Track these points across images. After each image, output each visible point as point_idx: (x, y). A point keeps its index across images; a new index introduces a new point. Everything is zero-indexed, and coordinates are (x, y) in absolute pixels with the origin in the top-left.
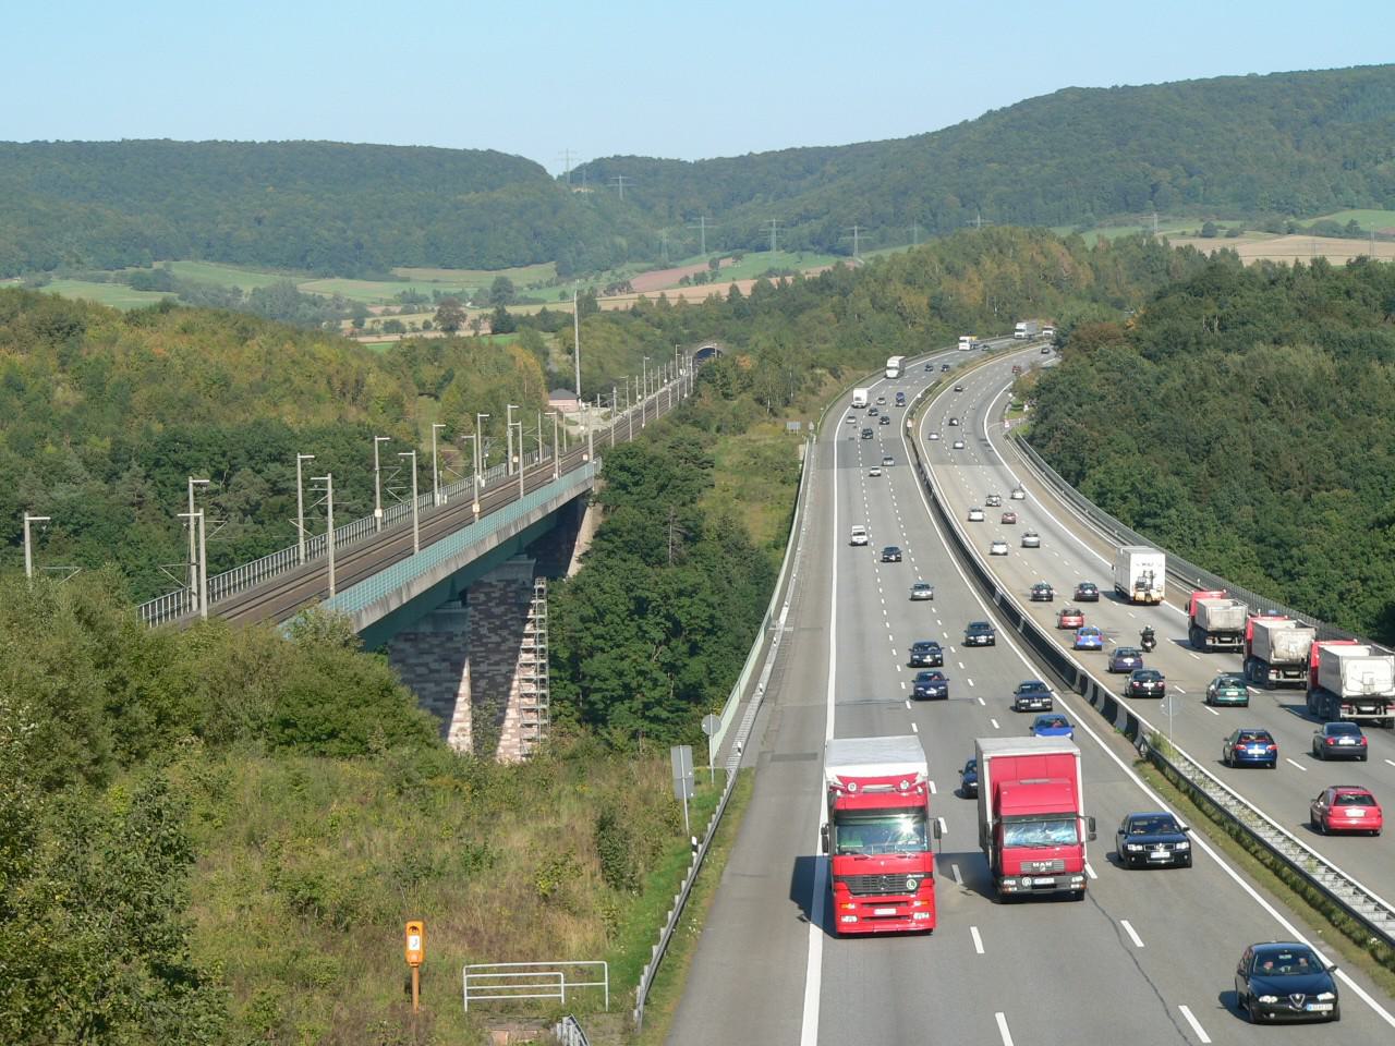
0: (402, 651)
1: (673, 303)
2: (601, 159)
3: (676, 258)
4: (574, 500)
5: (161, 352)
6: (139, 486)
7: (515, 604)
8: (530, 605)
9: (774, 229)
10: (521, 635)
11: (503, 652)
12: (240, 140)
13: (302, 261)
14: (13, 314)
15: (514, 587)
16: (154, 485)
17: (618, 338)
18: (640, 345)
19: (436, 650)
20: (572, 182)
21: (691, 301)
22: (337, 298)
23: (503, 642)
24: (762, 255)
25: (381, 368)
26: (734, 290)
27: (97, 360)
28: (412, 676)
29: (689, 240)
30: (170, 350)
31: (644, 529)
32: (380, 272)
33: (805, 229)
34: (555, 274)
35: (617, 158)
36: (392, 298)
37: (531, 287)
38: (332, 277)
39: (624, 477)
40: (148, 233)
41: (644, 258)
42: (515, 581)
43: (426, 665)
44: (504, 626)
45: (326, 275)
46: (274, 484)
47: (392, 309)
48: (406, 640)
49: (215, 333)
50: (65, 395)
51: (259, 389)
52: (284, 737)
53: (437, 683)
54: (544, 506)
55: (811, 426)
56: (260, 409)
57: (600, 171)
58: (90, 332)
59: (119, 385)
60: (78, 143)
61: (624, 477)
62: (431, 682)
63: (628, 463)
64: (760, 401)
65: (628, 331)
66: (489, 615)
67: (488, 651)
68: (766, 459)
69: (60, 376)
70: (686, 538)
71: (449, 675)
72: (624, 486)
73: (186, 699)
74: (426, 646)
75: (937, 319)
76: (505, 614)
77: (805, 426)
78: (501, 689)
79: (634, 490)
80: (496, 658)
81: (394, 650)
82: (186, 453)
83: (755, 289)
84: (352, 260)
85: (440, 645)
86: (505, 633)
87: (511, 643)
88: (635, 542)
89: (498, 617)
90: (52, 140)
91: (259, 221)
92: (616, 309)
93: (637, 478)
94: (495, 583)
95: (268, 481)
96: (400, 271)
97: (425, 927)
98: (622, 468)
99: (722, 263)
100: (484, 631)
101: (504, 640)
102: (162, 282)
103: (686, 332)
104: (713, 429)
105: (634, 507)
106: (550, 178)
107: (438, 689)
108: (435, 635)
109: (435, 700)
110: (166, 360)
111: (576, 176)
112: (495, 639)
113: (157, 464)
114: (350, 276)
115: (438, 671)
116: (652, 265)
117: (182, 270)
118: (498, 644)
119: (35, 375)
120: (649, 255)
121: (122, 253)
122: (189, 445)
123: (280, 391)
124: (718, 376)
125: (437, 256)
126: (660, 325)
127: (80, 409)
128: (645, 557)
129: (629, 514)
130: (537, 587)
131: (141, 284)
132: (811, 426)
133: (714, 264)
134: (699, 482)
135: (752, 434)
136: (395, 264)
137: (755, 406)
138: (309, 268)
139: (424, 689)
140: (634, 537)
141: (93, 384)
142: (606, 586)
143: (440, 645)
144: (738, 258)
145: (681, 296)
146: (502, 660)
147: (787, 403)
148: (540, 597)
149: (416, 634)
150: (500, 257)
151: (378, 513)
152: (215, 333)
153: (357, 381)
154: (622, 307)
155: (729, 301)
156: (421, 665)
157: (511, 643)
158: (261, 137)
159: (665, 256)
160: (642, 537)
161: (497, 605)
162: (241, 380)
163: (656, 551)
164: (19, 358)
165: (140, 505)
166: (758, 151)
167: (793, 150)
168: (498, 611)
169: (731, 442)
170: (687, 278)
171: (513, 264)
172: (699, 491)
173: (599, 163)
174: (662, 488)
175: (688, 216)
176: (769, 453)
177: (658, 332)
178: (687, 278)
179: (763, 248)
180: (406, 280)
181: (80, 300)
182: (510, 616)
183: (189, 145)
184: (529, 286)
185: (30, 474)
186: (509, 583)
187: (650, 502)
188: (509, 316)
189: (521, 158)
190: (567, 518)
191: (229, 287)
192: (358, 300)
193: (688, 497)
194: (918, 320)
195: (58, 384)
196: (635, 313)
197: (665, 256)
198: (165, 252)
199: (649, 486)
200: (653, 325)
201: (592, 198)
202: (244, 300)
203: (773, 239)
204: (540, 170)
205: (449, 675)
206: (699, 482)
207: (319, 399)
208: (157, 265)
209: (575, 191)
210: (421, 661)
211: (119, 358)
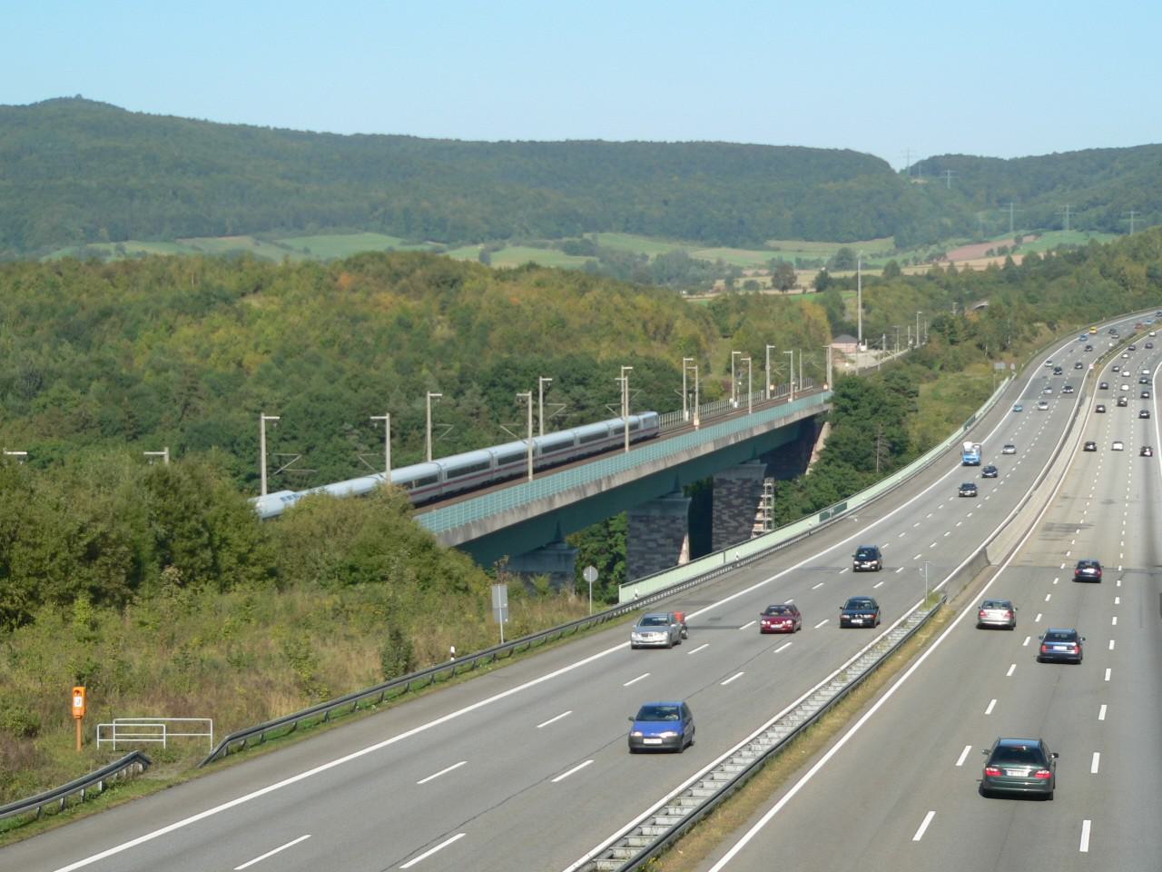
0: (639, 529)
1: (960, 270)
2: (935, 157)
3: (990, 233)
4: (811, 418)
5: (515, 300)
6: (476, 400)
7: (750, 498)
8: (761, 499)
9: (1068, 213)
10: (752, 522)
11: (738, 534)
13: (698, 234)
14: (413, 271)
15: (749, 484)
16: (491, 400)
17: (911, 297)
18: (929, 302)
19: (663, 529)
20: (912, 174)
21: (977, 269)
22: (720, 262)
24: (1057, 234)
25: (687, 316)
26: (1009, 262)
27: (467, 306)
29: (1001, 221)
30: (523, 300)
31: (857, 443)
32: (756, 242)
33: (1092, 213)
34: (893, 247)
35: (948, 156)
36: (764, 263)
37: (873, 256)
38: (720, 246)
39: (845, 402)
40: (581, 211)
41: (965, 234)
42: (749, 480)
43: (655, 540)
44: (741, 514)
45: (715, 245)
46: (578, 401)
47: (760, 272)
48: (641, 521)
49: (561, 287)
50: (442, 331)
51: (587, 330)
52: (351, 579)
53: (664, 555)
54: (771, 423)
55: (1013, 367)
56: (586, 344)
57: (933, 166)
58: (467, 285)
59: (481, 325)
60: (533, 143)
61: (845, 402)
63: (849, 391)
64: (980, 346)
65: (920, 291)
66: (729, 505)
67: (729, 533)
68: (974, 391)
69: (440, 317)
70: (892, 450)
71: (671, 549)
72: (845, 410)
73: (261, 548)
74: (656, 526)
75: (1153, 285)
76: (742, 505)
77: (1008, 367)
79: (853, 412)
82: (514, 377)
83: (1025, 260)
87: (746, 528)
88: (849, 453)
89: (737, 507)
90: (513, 140)
91: (666, 203)
92: (916, 274)
93: (855, 403)
94: (734, 481)
95: (573, 399)
96: (773, 243)
97: (86, 692)
98: (844, 396)
99: (1026, 239)
100: (725, 517)
102: (588, 249)
103: (967, 292)
104: (937, 368)
105: (852, 426)
106: (893, 171)
108: (663, 518)
110: (519, 306)
111: (914, 171)
112: (734, 524)
113: (493, 384)
114: (734, 246)
116: (968, 240)
117: (606, 240)
118: (736, 528)
119: (421, 317)
120: (968, 232)
121: (561, 226)
122: (515, 369)
123: (601, 332)
124: (947, 326)
125: (801, 231)
126: (947, 287)
127: (450, 342)
128: (856, 466)
129: (849, 431)
130: (766, 485)
131: (571, 250)
132: (1013, 367)
134: (904, 408)
135: (967, 373)
136: (768, 237)
137: (976, 350)
138: (702, 239)
140: (848, 449)
141: (463, 324)
142: (822, 486)
144: (1038, 235)
145: (967, 265)
147: (1004, 348)
148: (769, 493)
149: (648, 517)
150: (850, 232)
152: (561, 287)
153: (667, 326)
154: (920, 272)
155: (1005, 269)
157: (746, 528)
158: (671, 138)
159: (980, 233)
160: (855, 449)
161: (737, 498)
162: (575, 322)
163: (865, 460)
164: (412, 304)
165: (477, 415)
166: (1061, 151)
167: (1089, 150)
168: (736, 502)
169: (950, 377)
170: (992, 251)
171: (861, 238)
172: (904, 415)
173: (934, 160)
174: (875, 411)
175: (1002, 201)
176: (977, 387)
177: (945, 292)
178: (992, 251)
179: (1058, 228)
180: (777, 249)
182: (746, 506)
183: (617, 144)
184: (872, 255)
185: (397, 390)
186: (745, 481)
187: (865, 423)
188: (830, 279)
189: (871, 156)
190: (808, 428)
191: (639, 253)
192: (736, 264)
193: (894, 419)
194: (1137, 286)
195: (439, 322)
196: (929, 277)
197: (980, 233)
198: (593, 225)
199: (865, 409)
200: (942, 287)
201: (926, 187)
202: (649, 263)
203: (1066, 221)
204: (885, 165)
205: (671, 549)
206: (904, 408)
207: (632, 338)
208: (587, 236)
209: (913, 181)
211: (485, 304)
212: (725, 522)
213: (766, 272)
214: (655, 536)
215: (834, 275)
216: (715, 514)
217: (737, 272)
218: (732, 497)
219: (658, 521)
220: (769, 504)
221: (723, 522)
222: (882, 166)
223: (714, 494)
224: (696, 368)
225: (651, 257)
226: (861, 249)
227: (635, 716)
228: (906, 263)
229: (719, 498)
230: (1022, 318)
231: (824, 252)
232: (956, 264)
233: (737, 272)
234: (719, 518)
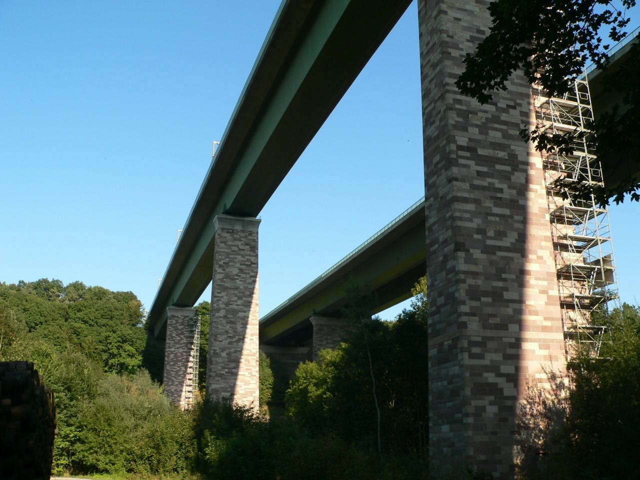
0: (226, 237)
7: (188, 326)
11: (182, 344)
15: (187, 319)
23: (181, 340)
42: (188, 316)
43: (237, 246)
48: (227, 232)
53: (243, 256)
66: (176, 329)
74: (238, 237)
78: (179, 359)
80: (179, 346)
81: (221, 237)
85: (246, 237)
86: (182, 336)
89: (180, 330)
94: (179, 316)
100: (174, 335)
101: (182, 339)
107: (243, 259)
108: (243, 232)
109: (241, 265)
115: (244, 250)
118: (179, 341)
139: (236, 258)
143: (246, 237)
146: (180, 347)
149: (233, 230)
161: (180, 325)
181: (42, 279)
210: (235, 244)
212: (174, 337)
216: (168, 333)
219: (239, 233)
221: (173, 337)
227: (611, 255)
229: (171, 325)
230: (70, 434)
234: (171, 335)
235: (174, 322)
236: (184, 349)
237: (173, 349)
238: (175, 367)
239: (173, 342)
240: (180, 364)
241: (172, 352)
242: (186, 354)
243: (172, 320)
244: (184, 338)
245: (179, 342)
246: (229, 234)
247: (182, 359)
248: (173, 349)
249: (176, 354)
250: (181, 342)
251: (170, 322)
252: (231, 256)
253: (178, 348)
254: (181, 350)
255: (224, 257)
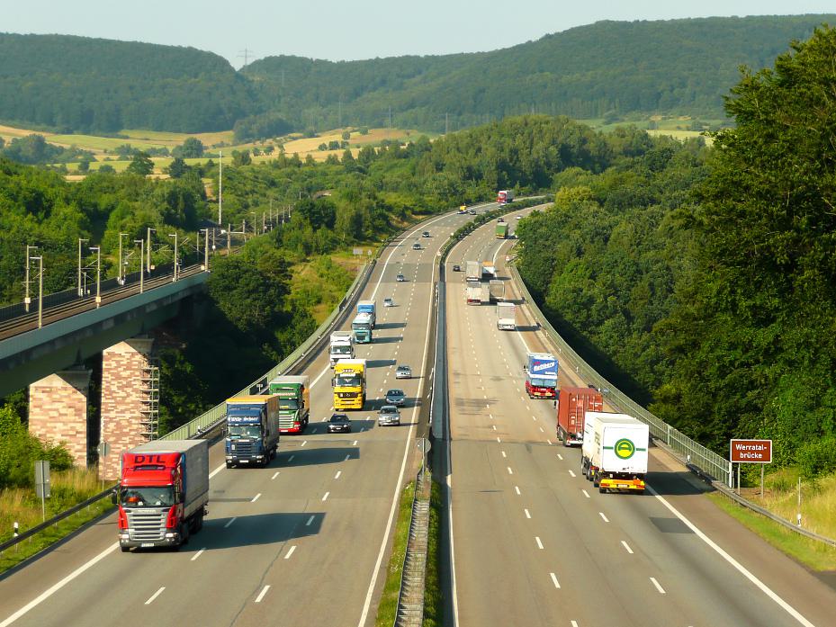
0: (41, 399)
12: (382, 57)
13: (49, 123)
19: (64, 400)
26: (348, 155)
28: (47, 418)
32: (112, 126)
36: (113, 150)
43: (57, 410)
47: (112, 157)
48: (43, 392)
62: (60, 422)
67: (117, 403)
80: (123, 407)
84: (84, 122)
86: (129, 390)
100: (114, 388)
101: (129, 395)
107: (65, 428)
111: (250, 69)
112: (124, 394)
115: (66, 415)
116: (302, 135)
118: (124, 398)
133: (347, 136)
146: (126, 410)
151: (98, 299)
156: (55, 410)
173: (269, 60)
180: (127, 138)
212: (114, 392)
213: (117, 157)
214: (57, 405)
215: (189, 162)
216: (104, 385)
217: (90, 157)
218: (121, 369)
219: (59, 392)
220: (156, 377)
221: (112, 392)
222: (219, 63)
223: (104, 366)
224: (41, 258)
225: (7, 141)
226: (207, 139)
228: (256, 153)
231: (175, 141)
232: (300, 155)
233: (90, 157)
235: (114, 364)
236: (134, 413)
237: (112, 414)
238: (118, 446)
239: (113, 401)
240: (127, 440)
241: (111, 420)
242: (137, 422)
243: (110, 362)
244: (134, 393)
245: (123, 401)
246: (46, 394)
247: (130, 430)
248: (112, 414)
249: (118, 423)
250: (128, 400)
251: (106, 365)
252: (48, 425)
253: (122, 412)
254: (128, 415)
255: (39, 427)
